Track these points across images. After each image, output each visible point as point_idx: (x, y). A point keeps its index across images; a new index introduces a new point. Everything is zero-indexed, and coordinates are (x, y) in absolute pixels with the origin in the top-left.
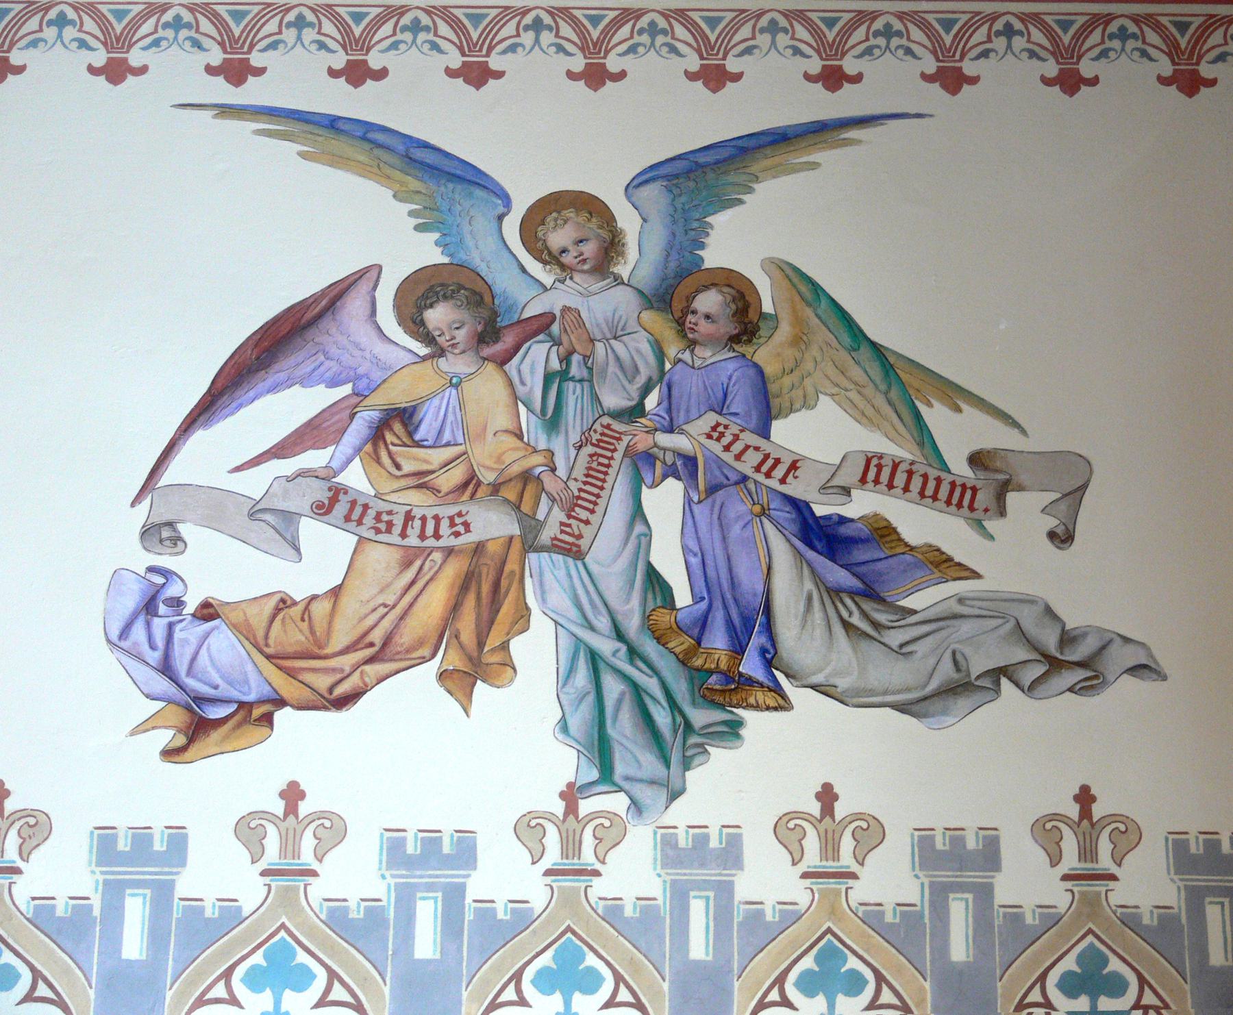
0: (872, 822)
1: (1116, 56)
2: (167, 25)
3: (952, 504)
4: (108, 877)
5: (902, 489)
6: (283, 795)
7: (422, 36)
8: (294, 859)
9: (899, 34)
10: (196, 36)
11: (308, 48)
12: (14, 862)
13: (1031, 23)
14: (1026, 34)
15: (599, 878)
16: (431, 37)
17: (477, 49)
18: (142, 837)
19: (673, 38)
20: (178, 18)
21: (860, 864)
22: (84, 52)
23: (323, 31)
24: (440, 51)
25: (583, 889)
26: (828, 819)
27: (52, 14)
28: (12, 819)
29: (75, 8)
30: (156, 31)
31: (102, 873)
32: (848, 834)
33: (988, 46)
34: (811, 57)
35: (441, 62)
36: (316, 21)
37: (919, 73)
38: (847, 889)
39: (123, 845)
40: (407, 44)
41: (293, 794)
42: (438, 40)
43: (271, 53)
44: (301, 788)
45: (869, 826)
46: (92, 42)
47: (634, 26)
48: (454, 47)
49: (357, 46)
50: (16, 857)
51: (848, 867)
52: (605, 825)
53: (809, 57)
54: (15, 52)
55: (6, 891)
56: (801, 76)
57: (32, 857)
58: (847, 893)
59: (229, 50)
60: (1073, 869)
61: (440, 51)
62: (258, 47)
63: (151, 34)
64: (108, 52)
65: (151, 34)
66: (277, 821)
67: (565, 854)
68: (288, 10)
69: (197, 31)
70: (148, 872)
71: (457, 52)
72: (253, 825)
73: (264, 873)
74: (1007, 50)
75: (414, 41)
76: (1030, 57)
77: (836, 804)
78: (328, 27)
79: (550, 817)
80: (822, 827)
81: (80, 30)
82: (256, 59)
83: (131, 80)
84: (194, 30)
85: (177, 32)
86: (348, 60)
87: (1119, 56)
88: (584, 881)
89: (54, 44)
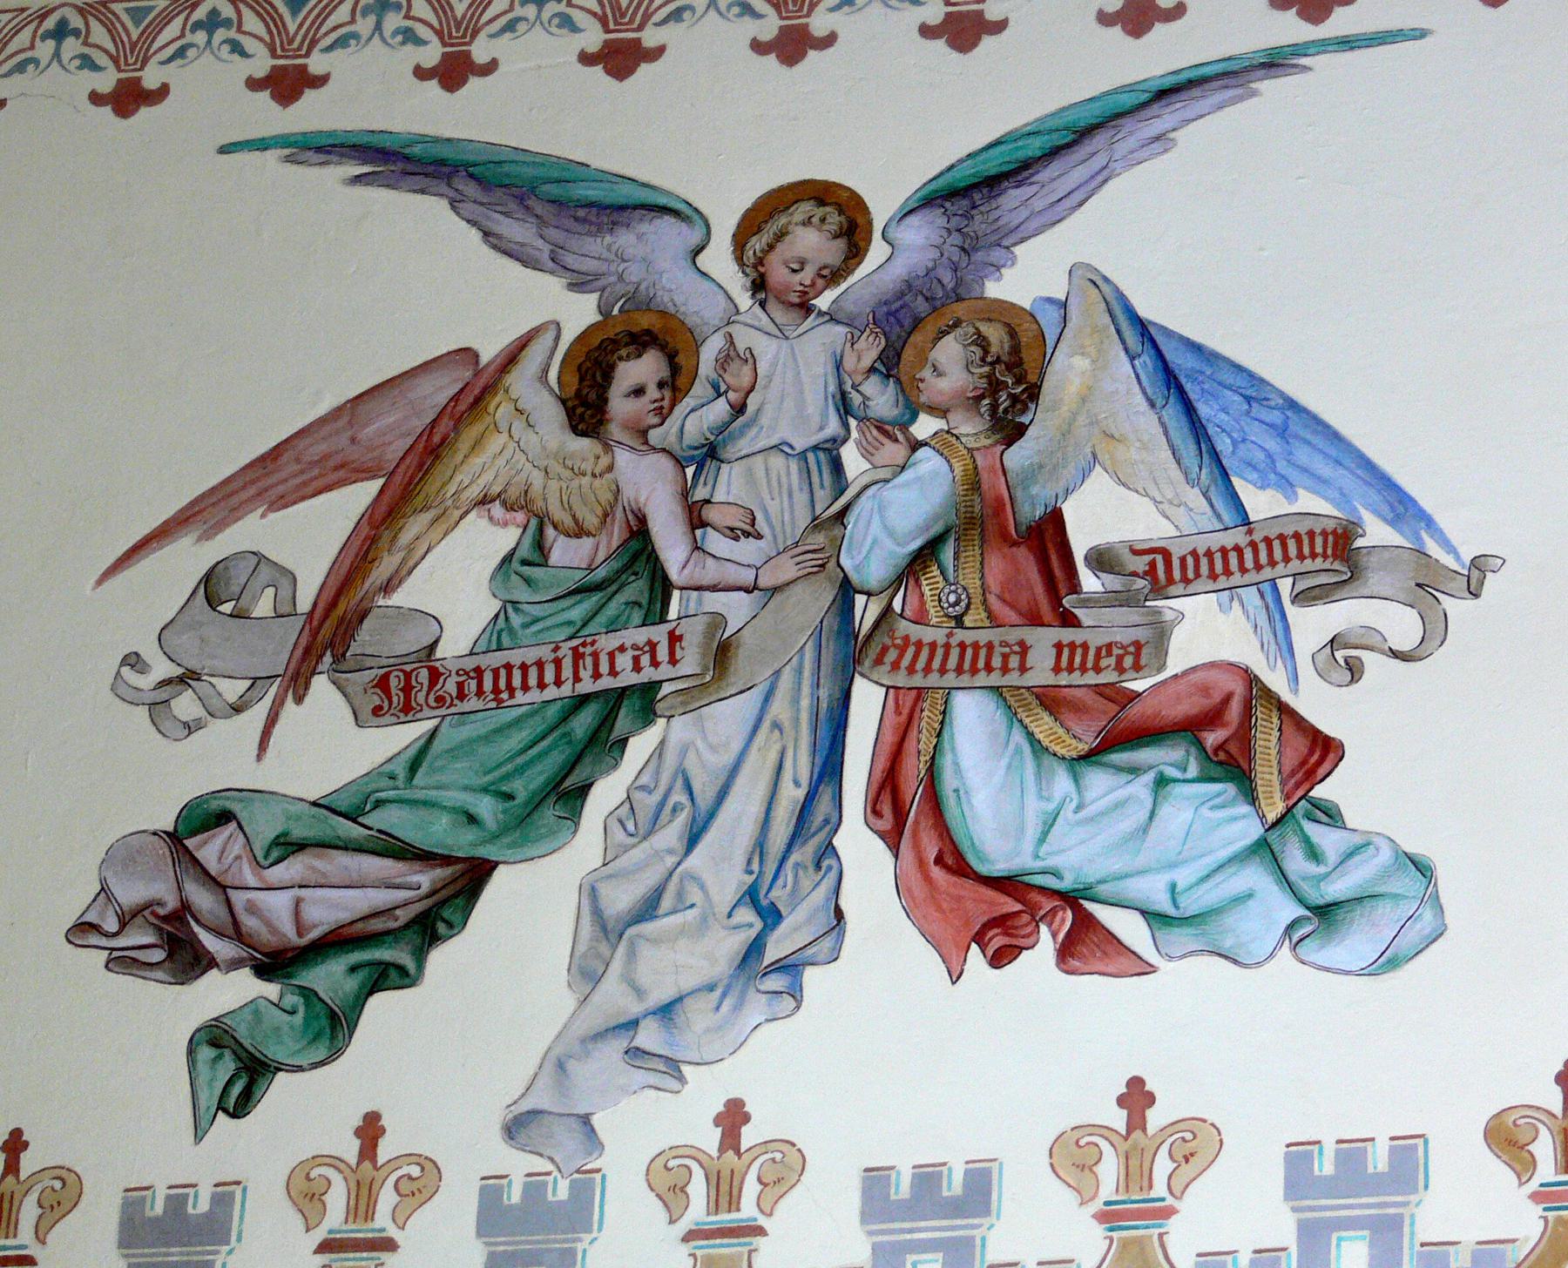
0: (428, 1165)
1: (526, 28)
2: (198, 26)
3: (932, 671)
4: (880, 1238)
5: (669, 663)
6: (1121, 1101)
7: (220, 34)
8: (7, 1237)
9: (227, 23)
10: (86, 50)
11: (390, 41)
12: (756, 1220)
13: (94, 16)
14: (83, 36)
15: (681, 1236)
16: (232, 34)
17: (627, 20)
18: (1352, 1151)
19: (239, 30)
20: (214, 12)
21: (399, 1228)
22: (409, 47)
23: (243, 29)
24: (244, 54)
25: (1156, 1237)
26: (367, 1165)
27: (200, 13)
28: (31, 1182)
29: (81, 11)
30: (182, 35)
31: (126, 1256)
32: (33, 1197)
33: (29, 54)
34: (105, 68)
35: (751, 29)
36: (234, 16)
37: (411, 68)
38: (750, 1252)
39: (1326, 1166)
40: (198, 48)
41: (370, 1130)
42: (570, 11)
43: (339, 53)
44: (1124, 1090)
45: (1080, 1147)
46: (102, 59)
47: (187, 19)
48: (262, 45)
49: (458, 30)
50: (755, 1212)
51: (383, 1230)
52: (1187, 1138)
53: (425, 43)
54: (316, 54)
55: (746, 1257)
56: (916, 34)
57: (49, 1238)
58: (749, 1257)
59: (279, 50)
60: (697, 1224)
61: (244, 54)
62: (657, 18)
63: (505, 12)
64: (608, 31)
65: (505, 12)
66: (1114, 1138)
67: (715, 1206)
68: (44, 16)
69: (239, 30)
70: (1364, 1205)
71: (598, 26)
72: (1082, 1143)
73: (689, 1237)
74: (52, 60)
75: (209, 42)
76: (233, 51)
77: (745, 1130)
78: (99, 34)
79: (1105, 1131)
80: (1123, 1146)
81: (86, 43)
82: (317, 63)
83: (474, 83)
84: (235, 29)
85: (211, 34)
86: (781, 27)
87: (530, 29)
88: (745, 1244)
89: (48, 66)
